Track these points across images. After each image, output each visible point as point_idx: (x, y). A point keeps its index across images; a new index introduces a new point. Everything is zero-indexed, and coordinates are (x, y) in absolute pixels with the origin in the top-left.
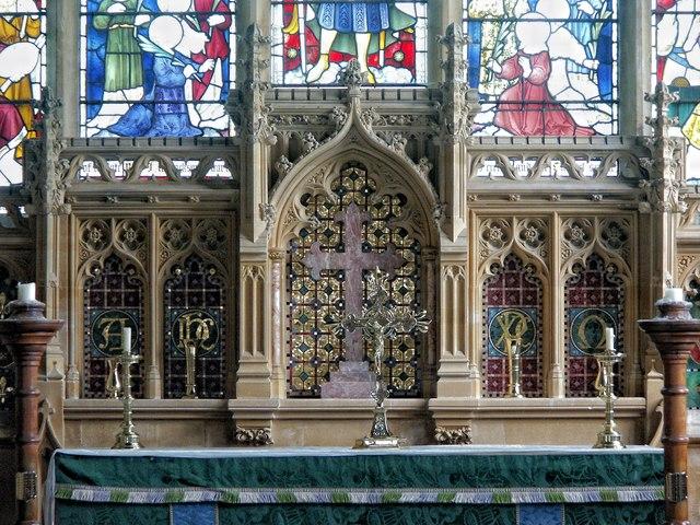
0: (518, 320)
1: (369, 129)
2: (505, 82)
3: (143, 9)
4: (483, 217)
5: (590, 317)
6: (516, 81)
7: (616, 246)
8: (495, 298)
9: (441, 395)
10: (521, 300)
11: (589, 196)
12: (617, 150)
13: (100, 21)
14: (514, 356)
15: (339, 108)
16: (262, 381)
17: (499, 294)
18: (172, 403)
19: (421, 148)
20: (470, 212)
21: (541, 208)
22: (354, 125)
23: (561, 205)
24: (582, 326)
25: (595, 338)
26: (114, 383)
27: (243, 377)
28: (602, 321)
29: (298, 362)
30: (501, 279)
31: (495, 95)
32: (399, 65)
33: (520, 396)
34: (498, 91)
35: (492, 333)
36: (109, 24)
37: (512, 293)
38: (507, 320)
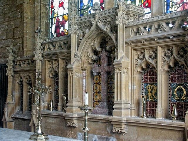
0: (153, 88)
1: (100, 25)
2: (178, 5)
3: (90, 6)
4: (136, 50)
5: (178, 87)
6: (182, 4)
7: (182, 57)
8: (146, 80)
9: (68, 112)
10: (154, 81)
11: (168, 38)
12: (180, 16)
13: (82, 11)
14: (143, 102)
15: (92, 20)
16: (119, 111)
17: (147, 78)
18: (168, 122)
19: (113, 29)
20: (131, 49)
21: (152, 44)
22: (97, 25)
23: (159, 43)
24: (176, 89)
25: (180, 95)
26: (51, 106)
27: (68, 106)
28: (183, 88)
29: (95, 101)
30: (148, 73)
31: (175, 11)
32: (147, 7)
33: (146, 117)
34: (176, 9)
35: (145, 93)
36: (84, 12)
37: (151, 78)
38: (150, 88)
